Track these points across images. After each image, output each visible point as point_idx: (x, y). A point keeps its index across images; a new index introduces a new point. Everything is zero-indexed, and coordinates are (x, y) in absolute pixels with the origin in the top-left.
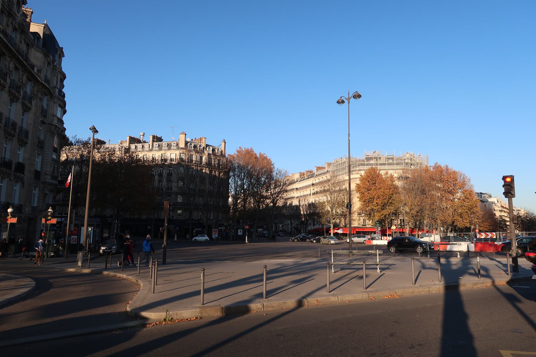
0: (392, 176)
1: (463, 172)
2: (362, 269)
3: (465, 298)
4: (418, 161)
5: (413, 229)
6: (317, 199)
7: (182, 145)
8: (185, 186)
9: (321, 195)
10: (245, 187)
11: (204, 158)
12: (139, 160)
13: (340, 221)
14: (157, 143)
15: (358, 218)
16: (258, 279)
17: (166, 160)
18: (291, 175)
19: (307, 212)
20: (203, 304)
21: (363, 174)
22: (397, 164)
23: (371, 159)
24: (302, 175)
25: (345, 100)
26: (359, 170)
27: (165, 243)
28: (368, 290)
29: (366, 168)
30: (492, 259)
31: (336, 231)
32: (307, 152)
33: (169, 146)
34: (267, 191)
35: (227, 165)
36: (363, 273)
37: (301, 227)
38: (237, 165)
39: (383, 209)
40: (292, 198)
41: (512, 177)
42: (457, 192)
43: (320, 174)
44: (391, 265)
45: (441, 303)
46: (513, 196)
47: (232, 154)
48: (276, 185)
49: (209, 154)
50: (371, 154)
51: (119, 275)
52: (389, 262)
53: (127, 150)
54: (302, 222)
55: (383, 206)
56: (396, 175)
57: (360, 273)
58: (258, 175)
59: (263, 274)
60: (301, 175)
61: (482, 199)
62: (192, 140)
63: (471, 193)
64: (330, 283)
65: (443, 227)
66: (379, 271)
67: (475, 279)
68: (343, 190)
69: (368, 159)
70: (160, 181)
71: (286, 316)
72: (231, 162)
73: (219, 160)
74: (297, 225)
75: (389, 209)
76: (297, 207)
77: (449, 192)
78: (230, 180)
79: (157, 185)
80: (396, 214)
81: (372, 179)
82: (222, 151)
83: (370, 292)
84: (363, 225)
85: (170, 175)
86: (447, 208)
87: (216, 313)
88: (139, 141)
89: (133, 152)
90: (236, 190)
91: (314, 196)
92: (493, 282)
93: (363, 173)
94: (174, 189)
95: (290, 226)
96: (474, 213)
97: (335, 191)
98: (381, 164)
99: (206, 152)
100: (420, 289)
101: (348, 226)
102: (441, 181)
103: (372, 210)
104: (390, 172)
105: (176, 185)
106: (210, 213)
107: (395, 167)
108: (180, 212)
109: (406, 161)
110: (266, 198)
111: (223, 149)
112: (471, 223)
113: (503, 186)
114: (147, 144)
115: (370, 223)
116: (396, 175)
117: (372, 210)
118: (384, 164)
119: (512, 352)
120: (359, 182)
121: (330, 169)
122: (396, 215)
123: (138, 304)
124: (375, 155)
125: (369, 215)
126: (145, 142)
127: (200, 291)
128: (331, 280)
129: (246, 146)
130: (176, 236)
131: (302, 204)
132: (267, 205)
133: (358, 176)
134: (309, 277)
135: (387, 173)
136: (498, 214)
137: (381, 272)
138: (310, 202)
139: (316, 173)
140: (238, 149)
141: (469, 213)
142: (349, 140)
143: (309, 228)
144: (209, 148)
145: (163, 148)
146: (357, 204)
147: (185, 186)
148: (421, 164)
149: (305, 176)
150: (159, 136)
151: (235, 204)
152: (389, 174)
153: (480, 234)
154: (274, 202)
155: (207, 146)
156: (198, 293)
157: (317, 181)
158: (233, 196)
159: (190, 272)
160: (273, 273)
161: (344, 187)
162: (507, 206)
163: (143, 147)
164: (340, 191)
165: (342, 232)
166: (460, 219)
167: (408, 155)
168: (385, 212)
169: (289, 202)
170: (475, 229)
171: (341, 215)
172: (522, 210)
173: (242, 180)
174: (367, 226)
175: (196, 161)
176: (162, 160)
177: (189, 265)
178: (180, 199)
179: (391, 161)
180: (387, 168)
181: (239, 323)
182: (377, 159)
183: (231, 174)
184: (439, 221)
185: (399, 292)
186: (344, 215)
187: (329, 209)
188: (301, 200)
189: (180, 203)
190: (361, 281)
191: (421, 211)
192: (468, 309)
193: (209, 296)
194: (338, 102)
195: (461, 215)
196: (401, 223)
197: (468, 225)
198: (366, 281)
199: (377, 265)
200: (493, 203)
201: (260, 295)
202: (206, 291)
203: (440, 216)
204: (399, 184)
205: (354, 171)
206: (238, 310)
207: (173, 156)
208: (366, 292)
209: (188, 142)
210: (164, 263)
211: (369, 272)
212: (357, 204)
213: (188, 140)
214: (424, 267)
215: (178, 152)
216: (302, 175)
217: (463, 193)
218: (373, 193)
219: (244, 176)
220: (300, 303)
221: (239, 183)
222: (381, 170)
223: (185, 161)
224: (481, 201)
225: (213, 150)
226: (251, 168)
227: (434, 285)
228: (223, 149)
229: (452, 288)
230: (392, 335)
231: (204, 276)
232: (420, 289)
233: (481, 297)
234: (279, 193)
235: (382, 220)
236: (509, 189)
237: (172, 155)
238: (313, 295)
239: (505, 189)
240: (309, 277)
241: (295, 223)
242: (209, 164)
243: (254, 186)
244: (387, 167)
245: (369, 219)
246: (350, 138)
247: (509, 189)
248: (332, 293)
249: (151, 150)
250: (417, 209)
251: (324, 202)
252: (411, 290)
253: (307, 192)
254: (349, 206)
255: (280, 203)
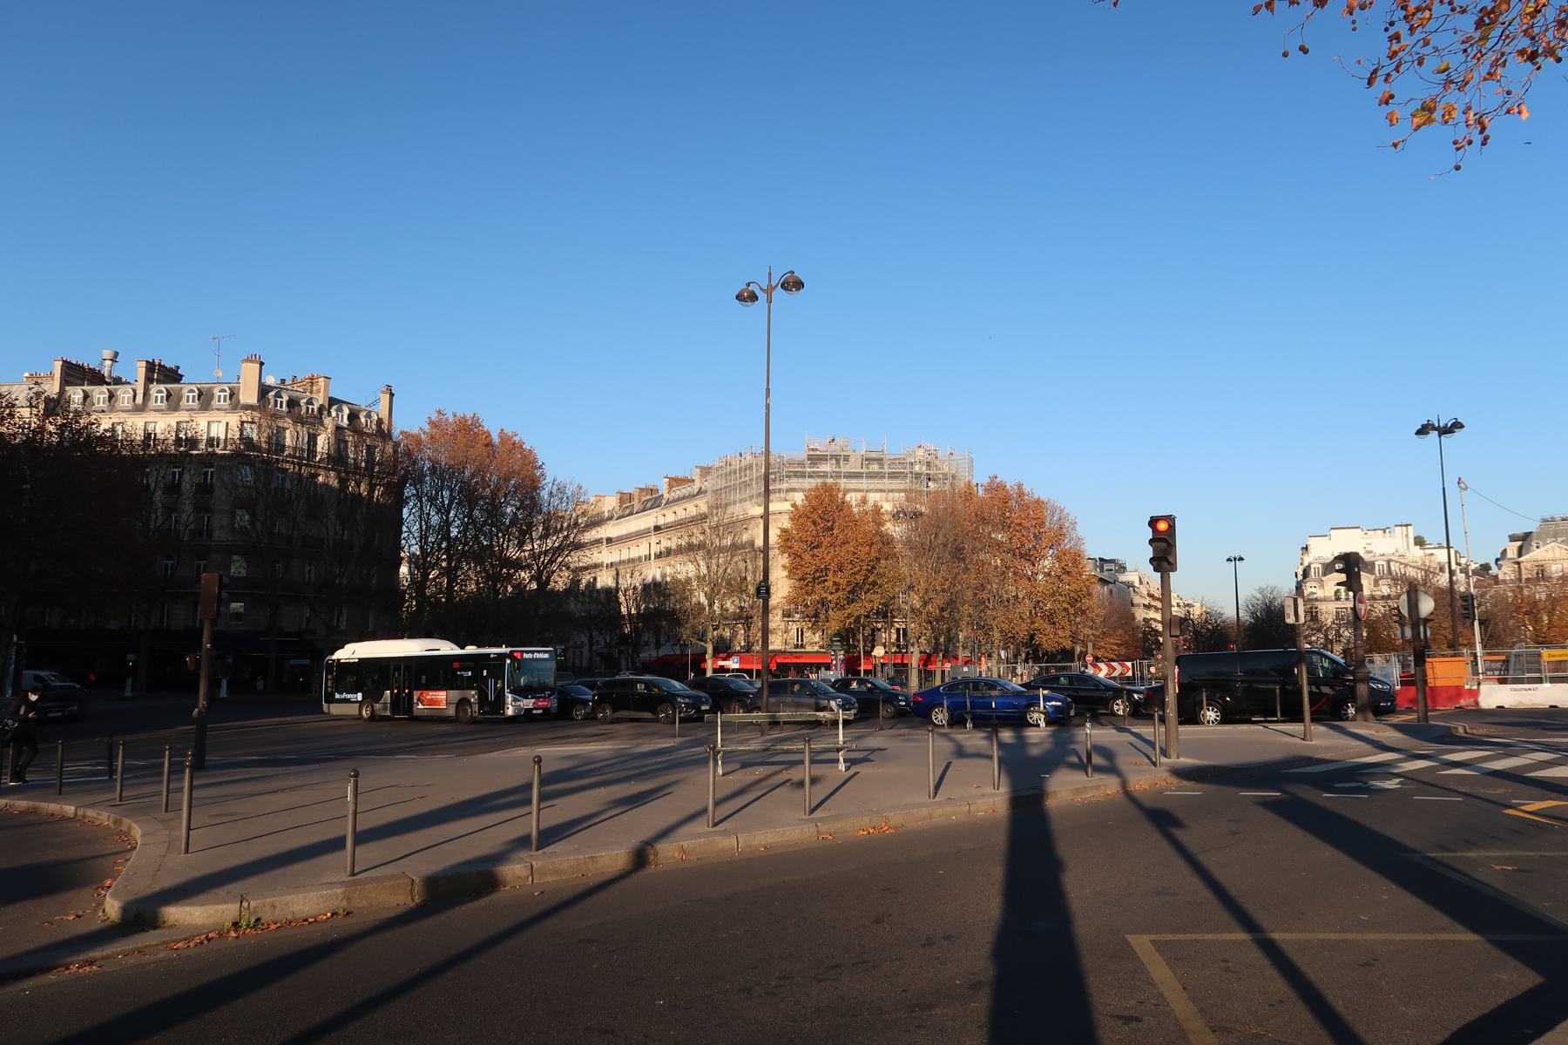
0: (877, 510)
1: (1060, 503)
2: (802, 762)
3: (1057, 826)
4: (946, 470)
5: (929, 656)
6: (668, 571)
7: (249, 396)
8: (258, 525)
9: (680, 558)
10: (454, 532)
11: (322, 442)
12: (101, 439)
13: (734, 634)
14: (162, 387)
15: (782, 626)
16: (515, 797)
17: (193, 442)
18: (592, 500)
19: (638, 607)
20: (353, 874)
21: (799, 503)
22: (893, 476)
23: (822, 458)
24: (626, 498)
25: (758, 292)
26: (788, 491)
27: (202, 702)
28: (815, 815)
29: (809, 483)
30: (1120, 729)
31: (720, 663)
32: (649, 436)
33: (205, 399)
34: (521, 545)
35: (395, 467)
36: (804, 772)
37: (620, 652)
38: (428, 464)
39: (853, 601)
40: (596, 566)
41: (1171, 520)
42: (1044, 557)
43: (679, 499)
44: (873, 750)
45: (1000, 839)
46: (1173, 567)
47: (415, 430)
48: (546, 529)
49: (338, 429)
50: (822, 446)
51: (53, 807)
52: (872, 742)
53: (54, 406)
54: (624, 639)
55: (852, 592)
56: (887, 507)
57: (795, 774)
58: (494, 494)
59: (529, 786)
60: (622, 501)
61: (1110, 569)
62: (283, 381)
63: (1077, 558)
64: (717, 804)
65: (1006, 648)
66: (842, 766)
67: (1079, 778)
68: (743, 547)
69: (815, 459)
70: (171, 509)
71: (619, 885)
72: (408, 453)
73: (370, 449)
74: (608, 645)
75: (870, 602)
76: (611, 594)
77: (1022, 556)
78: (405, 511)
79: (160, 521)
80: (886, 614)
81: (824, 517)
82: (380, 421)
83: (821, 820)
84: (797, 646)
85: (205, 489)
86: (1016, 597)
87: (399, 899)
88: (96, 378)
89: (78, 414)
90: (423, 538)
91: (660, 563)
92: (1124, 784)
93: (799, 498)
94: (219, 535)
95: (586, 649)
96: (1083, 612)
97: (721, 550)
98: (850, 476)
99: (327, 421)
100: (948, 809)
101: (757, 648)
102: (1005, 526)
103: (823, 602)
104: (873, 497)
105: (225, 523)
106: (340, 613)
107: (887, 483)
108: (236, 606)
109: (917, 468)
110: (518, 565)
111: (384, 415)
112: (1074, 638)
113: (1151, 542)
114: (129, 388)
115: (817, 638)
116: (887, 507)
117: (823, 602)
118: (857, 476)
119: (1153, 937)
120: (787, 524)
121: (707, 485)
122: (885, 616)
123: (144, 886)
124: (834, 449)
125: (815, 618)
126: (118, 381)
127: (343, 840)
128: (719, 795)
129: (457, 407)
130: (224, 683)
131: (624, 584)
132: (519, 587)
133: (787, 506)
134: (668, 785)
135: (864, 501)
136: (1140, 614)
137: (848, 769)
138: (649, 579)
139: (666, 496)
140: (434, 417)
141: (1072, 611)
142: (768, 406)
143: (644, 656)
144: (340, 410)
145: (184, 403)
146: (782, 586)
147: (258, 525)
148: (954, 477)
149: (635, 502)
150: (169, 364)
151: (419, 584)
152: (871, 503)
153: (1095, 666)
154: (542, 578)
155: (333, 401)
156: (337, 844)
157: (670, 518)
158: (412, 559)
159: (282, 790)
160: (558, 782)
161: (745, 537)
162: (1158, 594)
163: (111, 396)
164: (735, 547)
165: (737, 666)
166: (1049, 628)
167: (921, 452)
168: (857, 609)
169: (585, 579)
170: (1083, 655)
171: (737, 617)
172: (1198, 605)
173: (443, 510)
174: (809, 649)
175: (295, 449)
176: (178, 441)
177: (282, 770)
178: (238, 568)
179: (875, 467)
180: (865, 486)
181: (468, 920)
182: (838, 461)
183: (409, 491)
184: (996, 634)
185: (896, 818)
186: (744, 618)
187: (703, 599)
188: (622, 572)
189: (237, 579)
190: (798, 794)
191: (951, 605)
192: (1065, 849)
193: (371, 852)
194: (739, 297)
195: (1050, 618)
196: (898, 639)
197: (1067, 644)
198: (811, 794)
199: (838, 750)
200: (1130, 585)
201: (523, 842)
202: (362, 838)
203: (998, 619)
204: (894, 530)
205: (775, 491)
206: (468, 883)
207: (218, 431)
208: (811, 821)
209: (271, 388)
210: (199, 766)
211: (819, 770)
212: (782, 586)
213: (270, 380)
214: (961, 752)
215: (234, 419)
216: (626, 498)
217: (1059, 559)
218: (826, 555)
219: (451, 503)
220: (640, 858)
221: (435, 519)
222: (849, 491)
223: (259, 449)
224: (1101, 580)
225: (353, 416)
226: (473, 476)
227: (983, 797)
228: (384, 415)
229: (1028, 806)
230: (879, 920)
231: (356, 794)
232: (948, 809)
233: (1096, 820)
234: (558, 551)
235: (847, 630)
236: (1164, 554)
237: (214, 427)
238: (672, 837)
239: (1154, 551)
240: (668, 785)
241: (602, 641)
242: (337, 459)
243: (480, 530)
244: (864, 483)
245: (813, 629)
246: (772, 400)
247: (1164, 554)
248: (721, 827)
249: (139, 409)
250: (940, 600)
251: (688, 581)
252: (925, 812)
253: (639, 550)
254: (764, 590)
255: (560, 582)
